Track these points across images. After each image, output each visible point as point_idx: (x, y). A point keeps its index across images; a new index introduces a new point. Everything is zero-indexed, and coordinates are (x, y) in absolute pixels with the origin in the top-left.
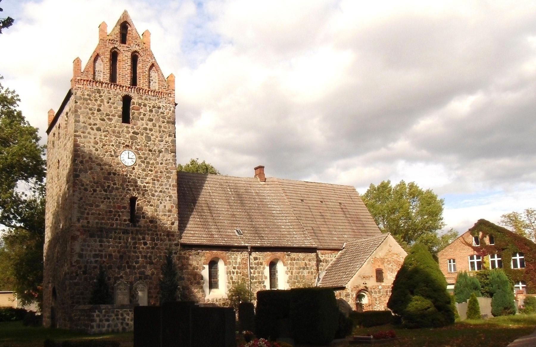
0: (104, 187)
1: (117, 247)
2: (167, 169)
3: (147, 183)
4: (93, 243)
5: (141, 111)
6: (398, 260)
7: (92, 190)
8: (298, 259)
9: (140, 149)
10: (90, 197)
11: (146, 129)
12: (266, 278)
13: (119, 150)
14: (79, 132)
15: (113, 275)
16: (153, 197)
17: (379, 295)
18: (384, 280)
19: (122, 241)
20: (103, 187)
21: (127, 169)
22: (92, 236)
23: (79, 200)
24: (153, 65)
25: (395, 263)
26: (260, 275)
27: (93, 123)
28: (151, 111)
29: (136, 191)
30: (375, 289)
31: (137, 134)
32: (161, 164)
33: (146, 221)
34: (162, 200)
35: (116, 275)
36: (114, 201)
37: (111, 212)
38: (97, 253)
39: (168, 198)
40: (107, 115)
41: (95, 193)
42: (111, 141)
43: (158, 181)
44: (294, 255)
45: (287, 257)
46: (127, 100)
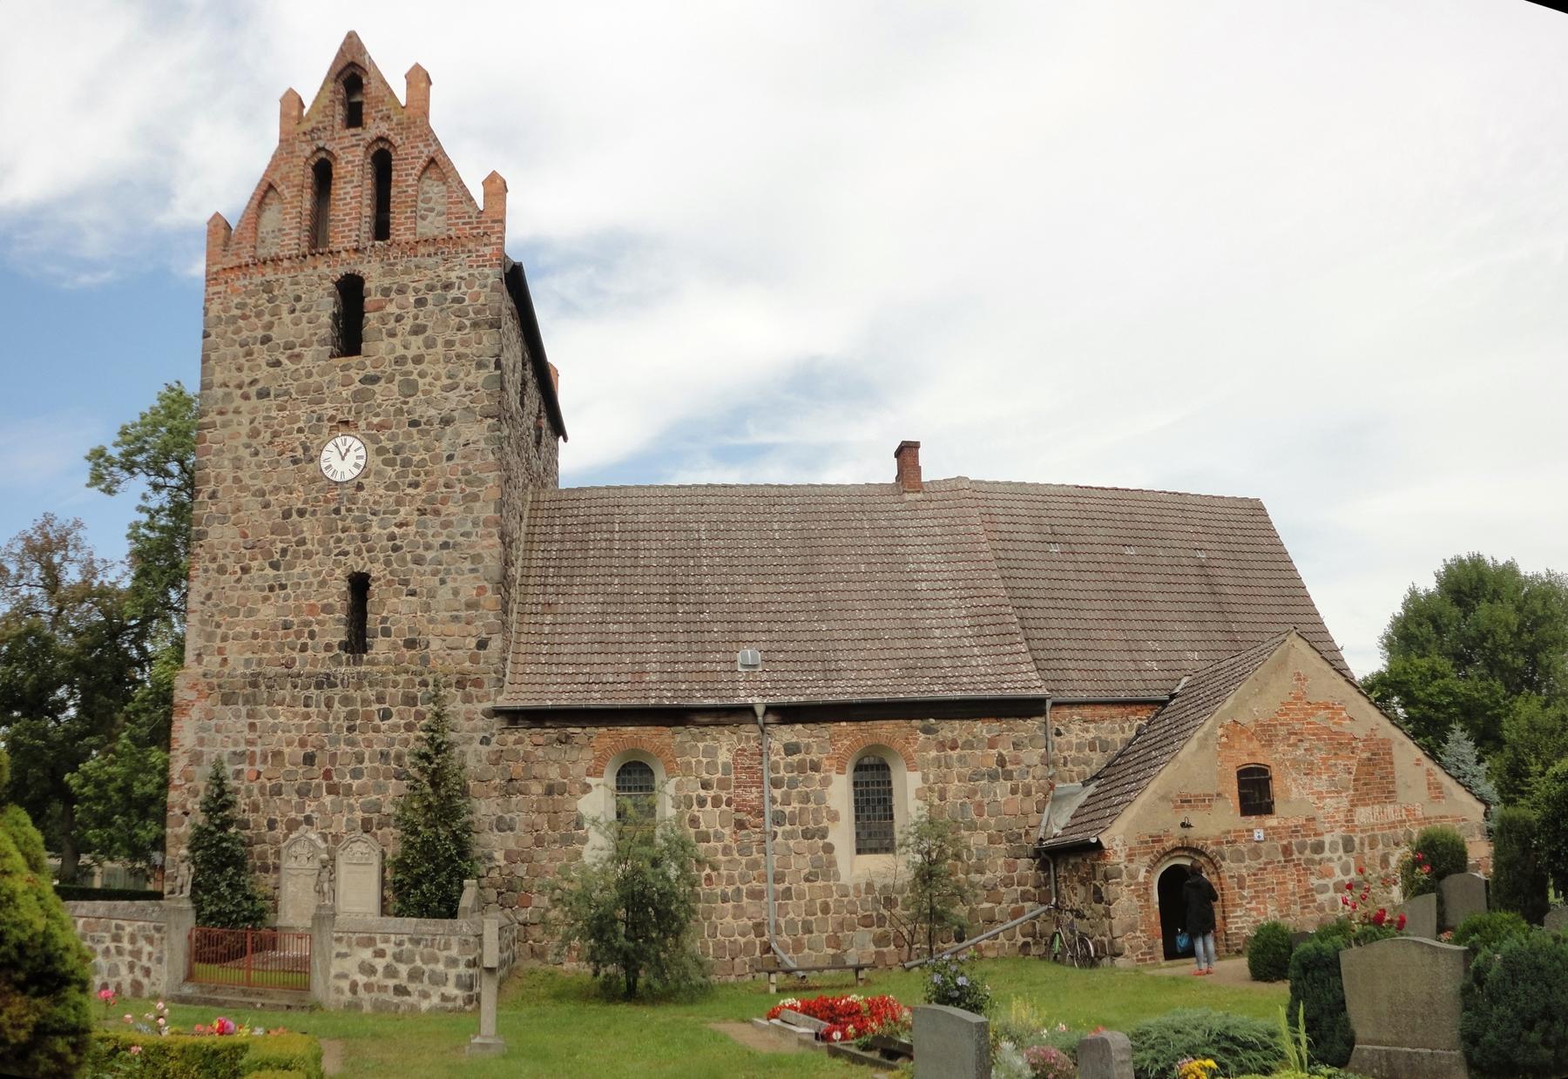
0: (272, 556)
1: (299, 728)
2: (467, 473)
3: (400, 525)
4: (229, 721)
5: (392, 308)
6: (1335, 728)
7: (237, 568)
8: (969, 745)
9: (380, 427)
10: (232, 589)
11: (400, 361)
12: (834, 817)
13: (317, 441)
14: (212, 414)
15: (283, 815)
16: (419, 567)
17: (1253, 863)
18: (1277, 807)
19: (313, 709)
20: (268, 554)
21: (339, 492)
22: (227, 700)
23: (203, 603)
24: (432, 161)
25: (1319, 739)
26: (812, 806)
27: (247, 380)
28: (421, 302)
29: (365, 554)
30: (1235, 841)
31: (374, 380)
32: (450, 458)
33: (394, 643)
34: (448, 572)
35: (293, 814)
36: (299, 592)
37: (287, 626)
38: (242, 748)
39: (467, 565)
40: (289, 346)
41: (246, 577)
42: (297, 419)
43: (437, 513)
44: (953, 729)
45: (922, 737)
46: (351, 291)
